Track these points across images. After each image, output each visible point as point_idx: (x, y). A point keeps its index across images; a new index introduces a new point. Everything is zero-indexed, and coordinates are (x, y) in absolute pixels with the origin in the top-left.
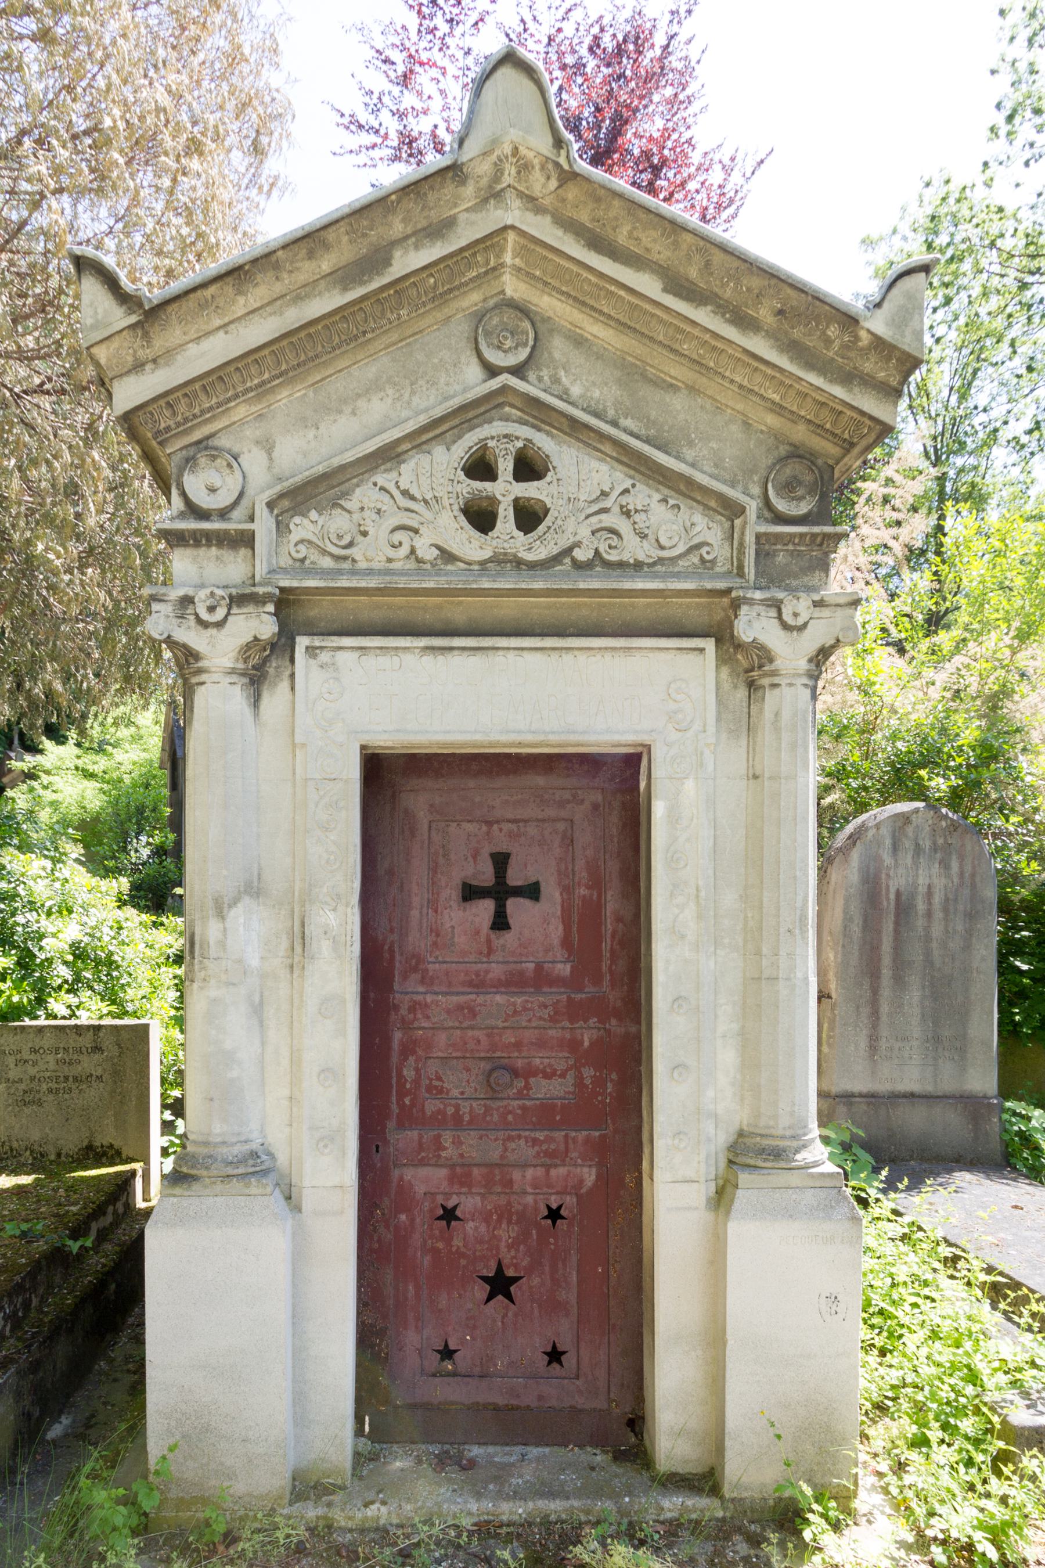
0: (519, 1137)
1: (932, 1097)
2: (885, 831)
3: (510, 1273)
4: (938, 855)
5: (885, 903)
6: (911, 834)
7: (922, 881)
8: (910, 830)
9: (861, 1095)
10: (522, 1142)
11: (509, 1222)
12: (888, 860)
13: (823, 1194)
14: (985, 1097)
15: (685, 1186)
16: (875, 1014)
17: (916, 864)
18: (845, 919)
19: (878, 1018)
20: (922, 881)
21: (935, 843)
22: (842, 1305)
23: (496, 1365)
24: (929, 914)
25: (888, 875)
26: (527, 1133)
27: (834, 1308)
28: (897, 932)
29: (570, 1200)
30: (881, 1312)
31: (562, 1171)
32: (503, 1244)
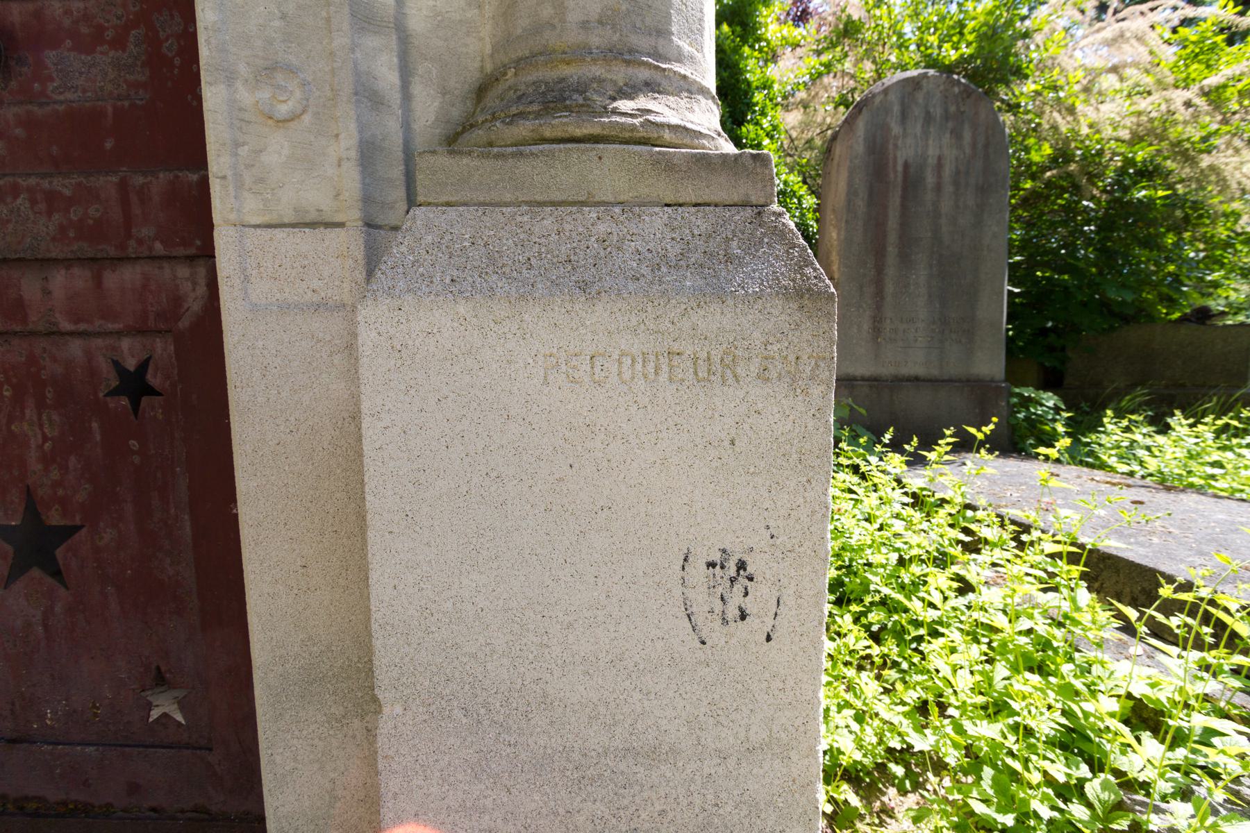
0: (15, 191)
1: (937, 381)
2: (892, 97)
3: (55, 518)
4: (950, 125)
5: (892, 175)
6: (921, 101)
7: (932, 152)
8: (920, 97)
9: (863, 379)
10: (22, 201)
11: (41, 406)
12: (896, 129)
13: (701, 222)
14: (992, 381)
15: (304, 240)
16: (879, 294)
17: (926, 134)
18: (848, 194)
19: (882, 298)
20: (932, 152)
21: (946, 111)
22: (762, 594)
23: (42, 717)
24: (938, 188)
25: (896, 146)
26: (32, 181)
27: (736, 599)
28: (904, 206)
29: (162, 348)
30: (884, 602)
31: (129, 275)
32: (32, 456)
